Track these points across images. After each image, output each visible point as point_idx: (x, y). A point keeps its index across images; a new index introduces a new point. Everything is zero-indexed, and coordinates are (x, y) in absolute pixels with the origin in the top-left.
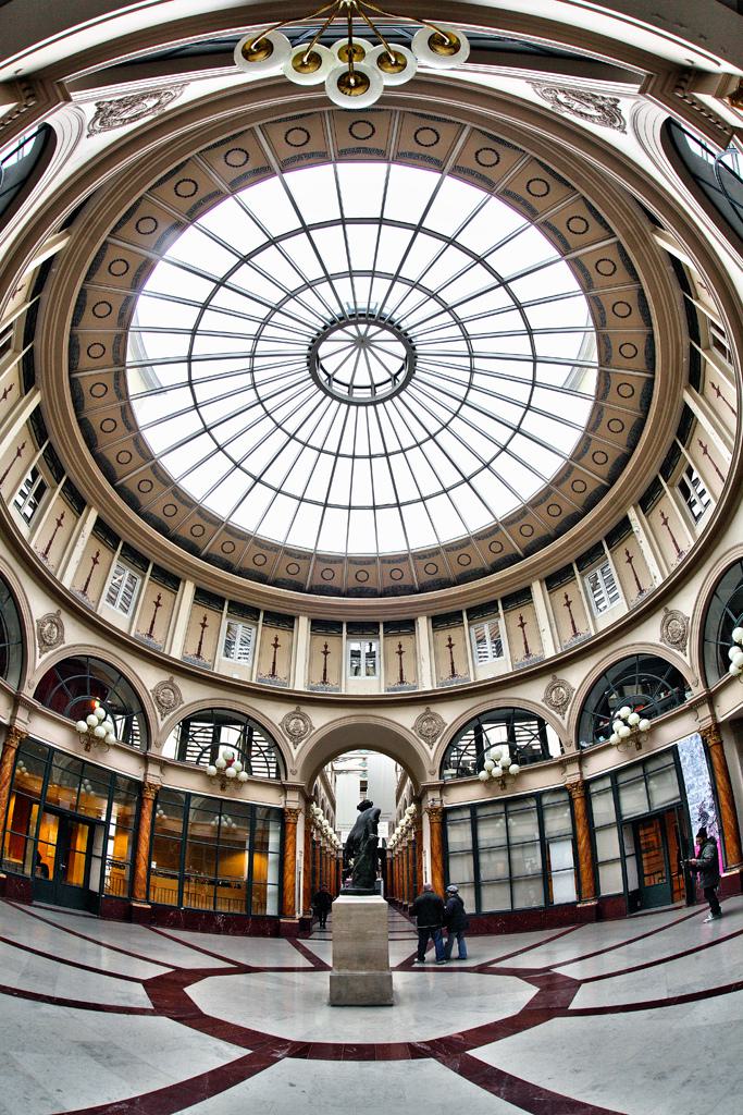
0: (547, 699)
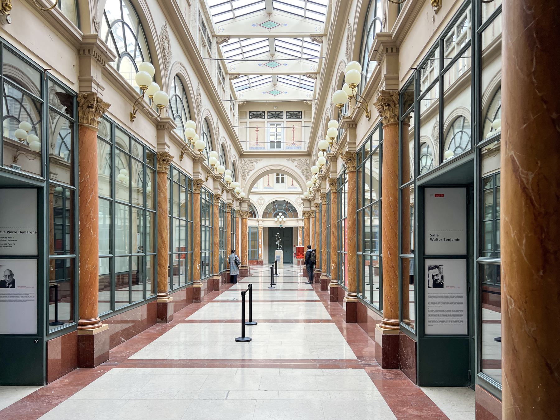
0: (257, 201)
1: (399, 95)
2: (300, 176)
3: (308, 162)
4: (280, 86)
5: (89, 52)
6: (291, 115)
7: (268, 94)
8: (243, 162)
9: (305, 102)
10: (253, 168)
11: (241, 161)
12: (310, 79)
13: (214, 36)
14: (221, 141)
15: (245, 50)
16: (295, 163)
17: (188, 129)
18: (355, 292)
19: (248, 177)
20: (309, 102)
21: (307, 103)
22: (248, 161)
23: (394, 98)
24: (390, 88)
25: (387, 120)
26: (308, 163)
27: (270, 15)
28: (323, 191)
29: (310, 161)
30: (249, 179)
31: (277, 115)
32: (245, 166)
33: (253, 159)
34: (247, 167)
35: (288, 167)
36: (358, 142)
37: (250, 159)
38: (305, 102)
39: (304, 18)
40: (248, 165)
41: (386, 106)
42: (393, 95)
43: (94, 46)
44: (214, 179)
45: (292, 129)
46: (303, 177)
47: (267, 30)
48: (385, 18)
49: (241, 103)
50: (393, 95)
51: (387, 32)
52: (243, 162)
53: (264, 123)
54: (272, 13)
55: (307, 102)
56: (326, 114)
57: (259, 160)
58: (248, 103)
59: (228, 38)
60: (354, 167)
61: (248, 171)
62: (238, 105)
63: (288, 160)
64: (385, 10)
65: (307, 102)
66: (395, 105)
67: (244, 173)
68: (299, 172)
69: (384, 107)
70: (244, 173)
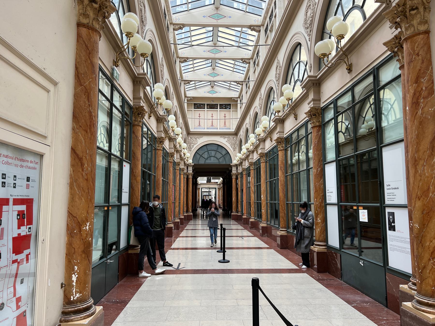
1: (321, 109)
2: (230, 149)
3: (235, 139)
4: (216, 88)
5: (140, 82)
6: (222, 106)
7: (208, 52)
8: (190, 138)
9: (233, 99)
10: (197, 143)
11: (188, 138)
12: (239, 85)
13: (178, 57)
14: (181, 126)
15: (195, 65)
16: (226, 139)
17: (171, 121)
18: (285, 228)
19: (193, 149)
20: (236, 99)
21: (234, 100)
22: (193, 138)
23: (318, 111)
24: (315, 105)
25: (314, 123)
26: (235, 139)
27: (217, 9)
28: (243, 167)
29: (236, 138)
30: (194, 150)
31: (212, 107)
32: (191, 141)
33: (196, 136)
34: (193, 142)
35: (208, 140)
36: (323, 100)
37: (195, 136)
38: (233, 99)
39: (188, 11)
40: (193, 141)
41: (313, 116)
42: (318, 110)
43: (143, 79)
44: (169, 140)
45: (226, 118)
46: (231, 149)
47: (213, 55)
48: (311, 67)
49: (189, 99)
50: (318, 110)
51: (313, 74)
52: (190, 138)
53: (204, 111)
54: (216, 44)
55: (235, 99)
56: (255, 110)
57: (201, 137)
58: (194, 98)
59: (187, 59)
60: (283, 147)
61: (193, 145)
62: (187, 100)
63: (221, 137)
64: (311, 62)
65: (235, 99)
66: (319, 115)
67: (190, 146)
68: (229, 145)
69: (312, 116)
70: (190, 146)
